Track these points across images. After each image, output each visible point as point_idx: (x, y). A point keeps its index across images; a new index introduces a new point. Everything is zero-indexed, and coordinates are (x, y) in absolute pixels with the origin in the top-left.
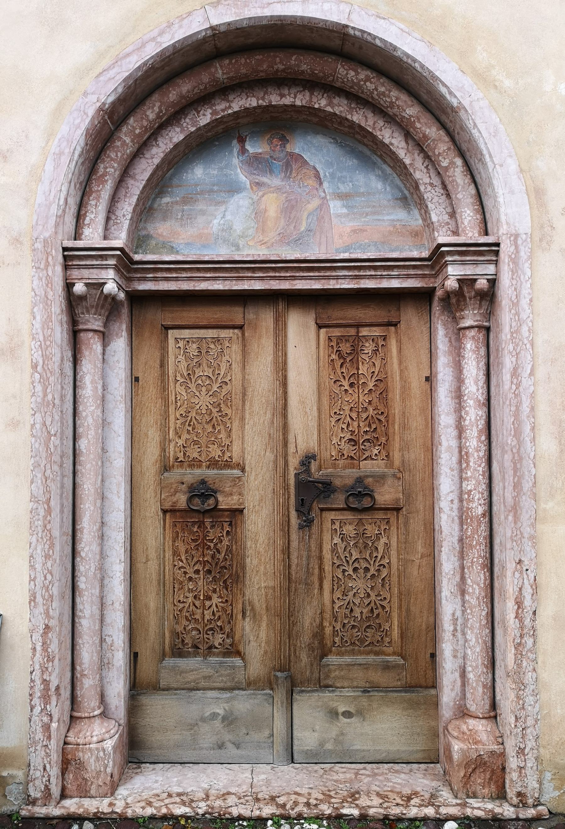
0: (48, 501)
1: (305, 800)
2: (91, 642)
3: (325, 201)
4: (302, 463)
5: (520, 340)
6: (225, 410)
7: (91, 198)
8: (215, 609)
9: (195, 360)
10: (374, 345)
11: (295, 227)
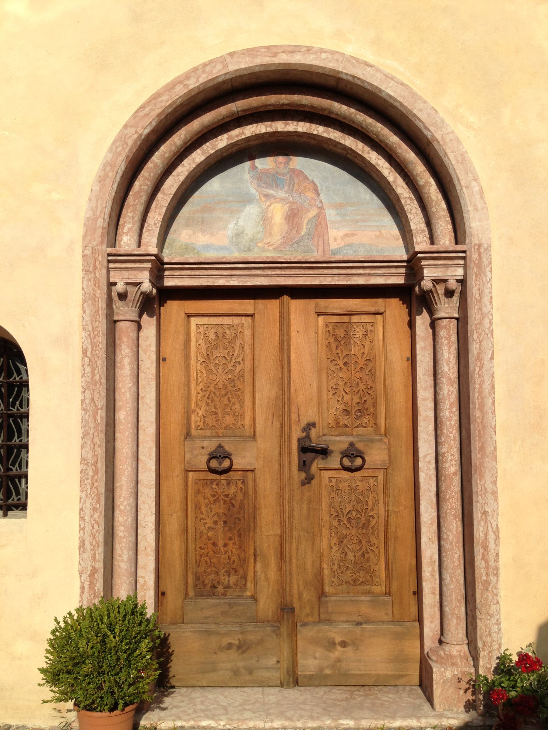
0: (95, 464)
1: (309, 714)
2: (128, 582)
3: (322, 210)
4: (304, 430)
5: (483, 330)
6: (238, 383)
7: (129, 211)
8: (230, 554)
9: (213, 343)
10: (364, 330)
11: (297, 231)
